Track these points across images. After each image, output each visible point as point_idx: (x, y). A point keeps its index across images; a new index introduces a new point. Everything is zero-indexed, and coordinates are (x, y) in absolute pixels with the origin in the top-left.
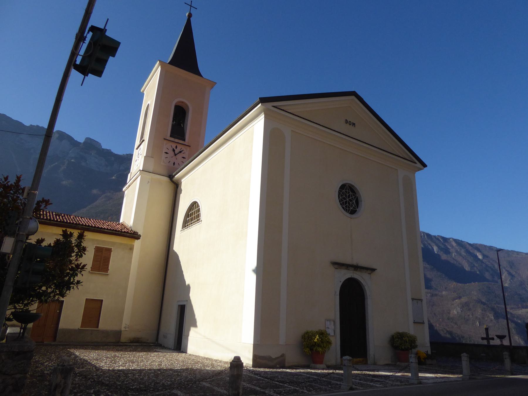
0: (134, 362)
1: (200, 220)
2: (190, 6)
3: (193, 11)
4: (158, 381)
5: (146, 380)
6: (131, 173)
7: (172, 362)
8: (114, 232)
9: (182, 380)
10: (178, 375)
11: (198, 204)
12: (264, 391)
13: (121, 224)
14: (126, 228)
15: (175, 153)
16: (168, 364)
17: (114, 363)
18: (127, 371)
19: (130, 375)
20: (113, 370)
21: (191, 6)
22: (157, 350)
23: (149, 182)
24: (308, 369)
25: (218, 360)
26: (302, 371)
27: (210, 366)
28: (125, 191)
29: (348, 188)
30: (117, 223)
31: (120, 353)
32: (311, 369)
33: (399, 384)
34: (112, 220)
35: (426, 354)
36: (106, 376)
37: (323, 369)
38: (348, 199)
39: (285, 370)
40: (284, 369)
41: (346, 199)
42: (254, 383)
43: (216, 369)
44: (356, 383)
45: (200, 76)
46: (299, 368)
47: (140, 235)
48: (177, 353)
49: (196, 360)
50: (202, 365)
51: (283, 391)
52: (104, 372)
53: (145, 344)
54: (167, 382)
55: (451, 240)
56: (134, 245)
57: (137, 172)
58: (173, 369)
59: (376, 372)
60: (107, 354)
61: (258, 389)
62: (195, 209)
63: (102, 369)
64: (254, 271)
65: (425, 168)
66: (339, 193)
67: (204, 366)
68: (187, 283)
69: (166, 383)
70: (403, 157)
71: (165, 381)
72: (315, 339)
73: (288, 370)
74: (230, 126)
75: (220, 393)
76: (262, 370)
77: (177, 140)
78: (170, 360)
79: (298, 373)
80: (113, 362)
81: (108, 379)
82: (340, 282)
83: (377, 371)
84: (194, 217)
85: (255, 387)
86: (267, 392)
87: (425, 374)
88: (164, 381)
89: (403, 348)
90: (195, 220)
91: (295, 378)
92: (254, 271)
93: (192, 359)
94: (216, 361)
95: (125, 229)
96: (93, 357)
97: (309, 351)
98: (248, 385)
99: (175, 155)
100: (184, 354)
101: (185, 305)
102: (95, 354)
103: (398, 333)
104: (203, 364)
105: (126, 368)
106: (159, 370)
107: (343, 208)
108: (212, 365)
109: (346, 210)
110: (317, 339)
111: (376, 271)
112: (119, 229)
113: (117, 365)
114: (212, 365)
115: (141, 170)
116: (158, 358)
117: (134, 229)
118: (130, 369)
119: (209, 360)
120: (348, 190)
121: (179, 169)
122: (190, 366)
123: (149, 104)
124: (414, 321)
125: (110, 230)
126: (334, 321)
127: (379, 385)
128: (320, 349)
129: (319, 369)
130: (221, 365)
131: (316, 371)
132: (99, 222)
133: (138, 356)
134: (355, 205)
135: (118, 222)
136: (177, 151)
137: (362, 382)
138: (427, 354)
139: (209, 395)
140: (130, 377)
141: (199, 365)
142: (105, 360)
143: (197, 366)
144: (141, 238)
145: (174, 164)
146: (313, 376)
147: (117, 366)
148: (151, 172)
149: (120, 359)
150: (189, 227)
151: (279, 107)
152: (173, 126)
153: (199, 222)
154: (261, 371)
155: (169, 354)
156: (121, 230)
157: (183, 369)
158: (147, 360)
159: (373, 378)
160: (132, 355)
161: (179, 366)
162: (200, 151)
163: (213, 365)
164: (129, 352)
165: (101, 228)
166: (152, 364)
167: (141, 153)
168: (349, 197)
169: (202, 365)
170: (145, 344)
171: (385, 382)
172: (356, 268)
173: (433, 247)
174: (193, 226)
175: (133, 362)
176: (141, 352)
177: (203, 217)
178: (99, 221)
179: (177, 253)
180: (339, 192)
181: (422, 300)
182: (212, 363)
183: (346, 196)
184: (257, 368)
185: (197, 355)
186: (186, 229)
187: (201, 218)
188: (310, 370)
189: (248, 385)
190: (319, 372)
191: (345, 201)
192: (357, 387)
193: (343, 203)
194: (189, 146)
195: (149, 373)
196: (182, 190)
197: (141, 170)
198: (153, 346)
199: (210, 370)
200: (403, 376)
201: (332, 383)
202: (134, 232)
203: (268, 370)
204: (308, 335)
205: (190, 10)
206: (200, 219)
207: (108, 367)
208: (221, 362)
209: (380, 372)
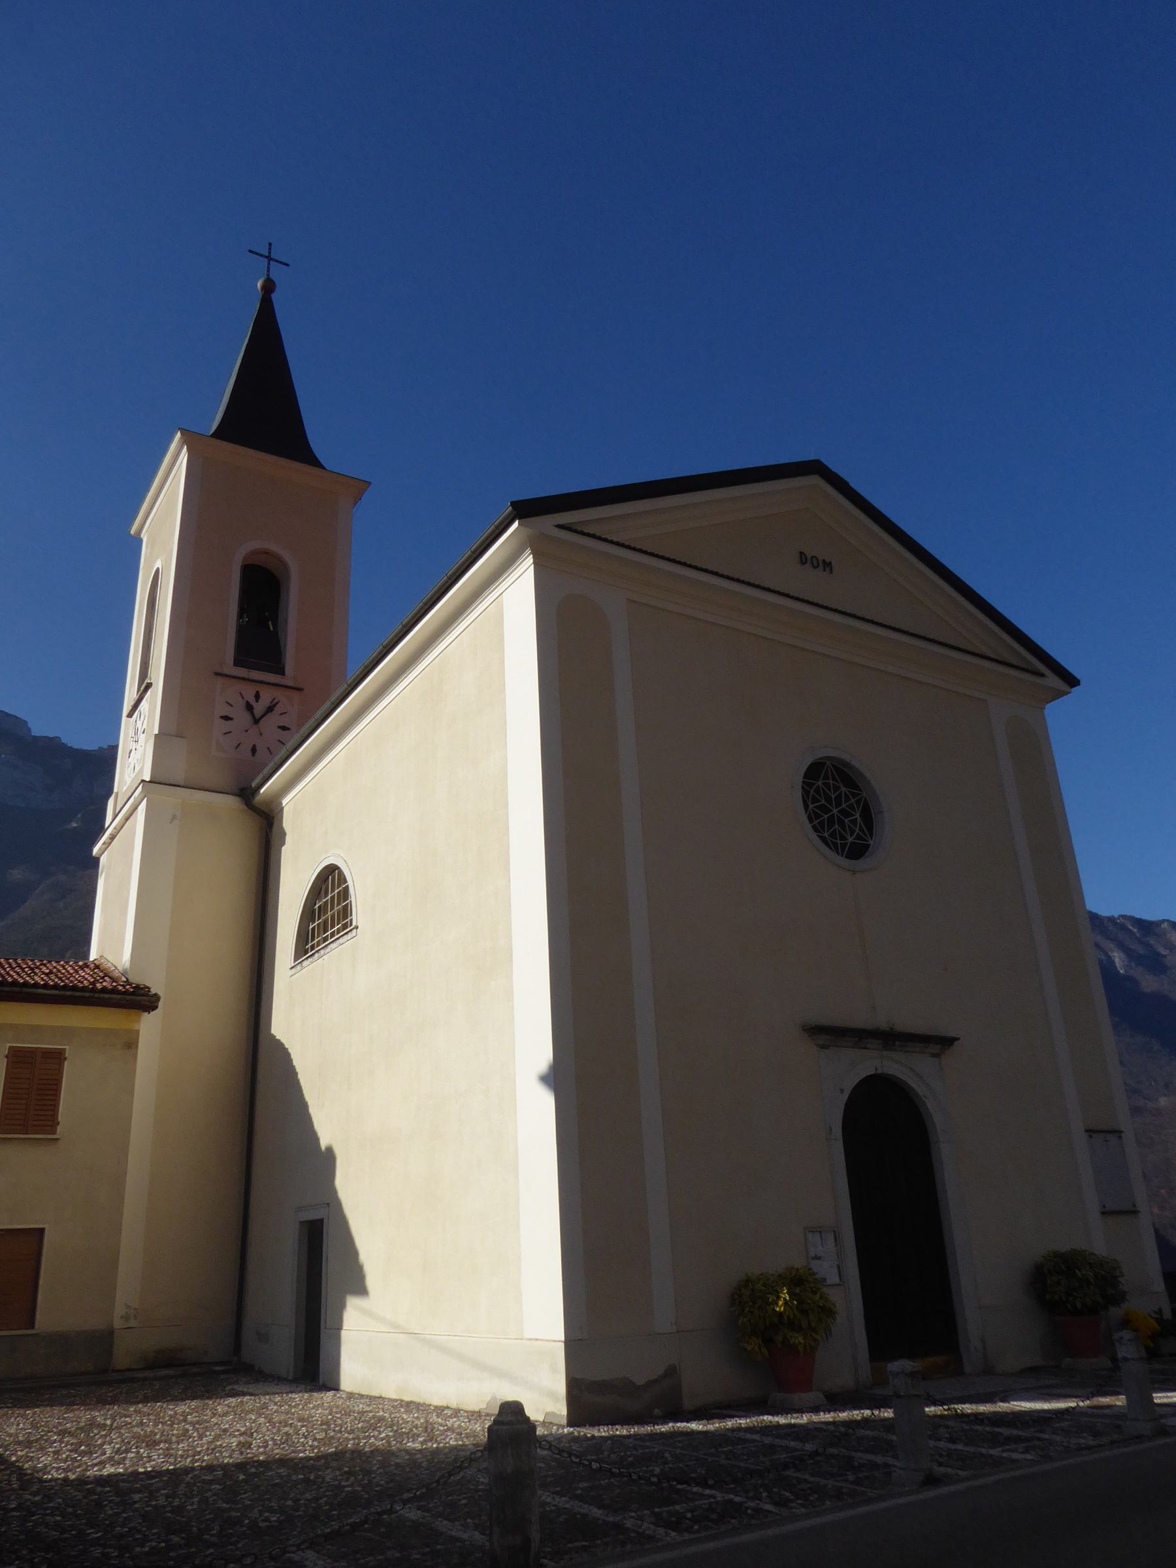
0: (155, 1441)
1: (351, 925)
2: (266, 257)
3: (277, 272)
4: (234, 1514)
5: (192, 1513)
6: (117, 794)
7: (287, 1429)
8: (69, 993)
9: (322, 1501)
10: (307, 1481)
11: (341, 873)
12: (618, 1519)
13: (92, 966)
14: (110, 977)
15: (253, 715)
16: (273, 1439)
17: (83, 1454)
18: (129, 1482)
19: (137, 1497)
20: (82, 1482)
21: (269, 258)
22: (236, 1387)
23: (174, 817)
24: (763, 1414)
25: (448, 1407)
26: (743, 1422)
27: (418, 1436)
28: (101, 855)
29: (832, 774)
30: (81, 963)
31: (108, 1411)
32: (772, 1415)
33: (1091, 1442)
34: (59, 956)
35: (1156, 1319)
36: (52, 1508)
37: (816, 1410)
38: (835, 811)
39: (685, 1424)
40: (682, 1422)
41: (830, 811)
42: (579, 1492)
43: (441, 1445)
44: (941, 1456)
45: (315, 465)
46: (733, 1413)
47: (156, 995)
48: (306, 1392)
49: (371, 1415)
50: (391, 1434)
51: (689, 1515)
52: (49, 1490)
53: (195, 1370)
54: (266, 1514)
55: (1165, 925)
56: (138, 1032)
57: (134, 788)
58: (292, 1460)
59: (1001, 1404)
60: (64, 1418)
61: (596, 1512)
62: (333, 890)
63: (41, 1481)
64: (545, 1079)
65: (1072, 689)
66: (806, 793)
67: (399, 1435)
68: (323, 1144)
69: (263, 1521)
70: (1000, 659)
71: (260, 1512)
72: (777, 1305)
73: (694, 1426)
74: (425, 604)
75: (458, 1544)
76: (603, 1434)
77: (256, 675)
78: (280, 1423)
79: (729, 1434)
80: (83, 1448)
81: (59, 1518)
82: (842, 1091)
83: (1004, 1400)
84: (333, 917)
85: (586, 1506)
86: (629, 1524)
87: (1169, 1394)
88: (256, 1510)
89: (1079, 1305)
90: (336, 927)
91: (723, 1457)
92: (545, 1079)
93: (359, 1413)
94: (440, 1410)
95: (105, 981)
96: (17, 1435)
97: (760, 1348)
98: (562, 1502)
99: (256, 721)
100: (331, 1393)
101: (322, 1221)
102: (24, 1424)
103: (1057, 1255)
104: (395, 1428)
105: (126, 1469)
106: (240, 1467)
107: (823, 839)
108: (428, 1428)
109: (834, 847)
110: (786, 1303)
111: (956, 1043)
112: (85, 982)
113: (97, 1457)
114: (426, 1431)
115: (148, 779)
116: (241, 1418)
117: (136, 979)
118: (141, 1470)
119: (418, 1410)
120: (834, 779)
121: (271, 765)
122: (350, 1440)
123: (158, 570)
124: (1104, 1206)
125: (56, 987)
126: (835, 1232)
127: (1022, 1453)
128: (798, 1339)
129: (801, 1411)
130: (460, 1426)
131: (793, 1421)
132: (19, 966)
133: (171, 1416)
134: (861, 829)
135: (82, 959)
136: (259, 708)
137: (960, 1447)
138: (1160, 1320)
139: (418, 1556)
140: (137, 1506)
141: (383, 1435)
142: (55, 1441)
143: (376, 1438)
144: (161, 1004)
145: (254, 750)
146: (784, 1442)
147: (96, 1465)
148: (179, 786)
149: (106, 1436)
150: (318, 951)
151: (579, 529)
152: (241, 631)
153: (347, 933)
154: (602, 1437)
155: (278, 1398)
156: (91, 983)
157: (325, 1457)
158: (201, 1431)
159: (997, 1430)
160: (149, 1415)
161: (310, 1443)
162: (333, 698)
163: (433, 1429)
164: (140, 1406)
165: (26, 984)
166: (218, 1443)
167: (145, 726)
168: (838, 804)
169: (391, 1434)
170: (195, 1370)
171: (1039, 1439)
172: (890, 1039)
173: (1110, 953)
174: (330, 947)
175: (152, 1444)
176: (183, 1400)
177: (359, 915)
178: (17, 963)
179: (282, 1044)
180: (803, 787)
181: (1122, 1132)
182: (427, 1421)
183: (828, 799)
184: (585, 1426)
185: (375, 1393)
186: (309, 960)
187: (354, 917)
188: (770, 1418)
189: (562, 1502)
190: (801, 1422)
191: (826, 816)
192: (950, 1470)
193: (822, 823)
194: (300, 690)
195: (204, 1481)
196: (284, 834)
197: (148, 779)
198: (223, 1372)
199: (420, 1451)
200: (1092, 1411)
201: (856, 1464)
202: (138, 987)
203: (625, 1432)
204: (753, 1290)
205: (268, 271)
206: (351, 920)
207: (66, 1470)
208: (457, 1412)
209: (1013, 1401)
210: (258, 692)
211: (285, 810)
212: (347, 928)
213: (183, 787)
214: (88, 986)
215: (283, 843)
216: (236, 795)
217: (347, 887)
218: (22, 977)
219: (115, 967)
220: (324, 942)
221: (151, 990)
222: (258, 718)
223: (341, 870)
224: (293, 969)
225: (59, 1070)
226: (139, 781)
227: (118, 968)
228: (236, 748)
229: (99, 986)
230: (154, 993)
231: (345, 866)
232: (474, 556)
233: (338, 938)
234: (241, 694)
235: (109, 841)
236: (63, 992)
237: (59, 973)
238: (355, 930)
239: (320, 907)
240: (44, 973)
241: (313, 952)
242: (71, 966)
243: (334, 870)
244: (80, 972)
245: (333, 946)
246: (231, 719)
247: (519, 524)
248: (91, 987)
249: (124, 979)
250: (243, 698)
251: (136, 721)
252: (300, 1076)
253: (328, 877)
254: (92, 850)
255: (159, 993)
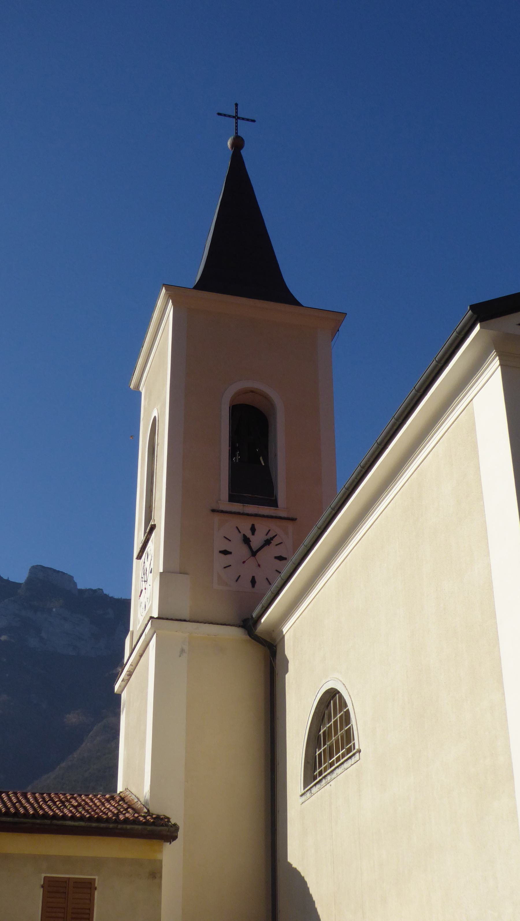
1: (354, 749)
8: (94, 825)
11: (341, 697)
13: (118, 798)
14: (133, 809)
21: (237, 118)
23: (182, 651)
28: (122, 692)
30: (107, 796)
47: (175, 825)
56: (161, 861)
62: (335, 715)
77: (251, 509)
84: (337, 742)
90: (341, 752)
95: (128, 812)
99: (254, 554)
112: (109, 814)
115: (156, 615)
117: (156, 810)
121: (269, 595)
123: (155, 417)
125: (82, 818)
132: (51, 799)
136: (256, 541)
144: (180, 834)
145: (253, 582)
148: (185, 621)
165: (55, 816)
167: (152, 566)
186: (318, 786)
187: (356, 741)
194: (293, 520)
197: (156, 615)
202: (158, 817)
205: (237, 130)
206: (354, 744)
210: (253, 526)
211: (286, 638)
212: (351, 751)
213: (189, 621)
214: (111, 818)
215: (287, 671)
216: (239, 627)
217: (348, 710)
218: (52, 810)
219: (138, 799)
220: (331, 767)
221: (171, 820)
222: (255, 550)
223: (341, 695)
224: (303, 796)
225: (90, 899)
226: (148, 618)
227: (141, 800)
228: (237, 581)
229: (121, 817)
230: (173, 823)
231: (343, 687)
232: (440, 365)
233: (343, 763)
234: (276, 545)
235: (127, 678)
236: (90, 824)
237: (86, 806)
238: (358, 754)
239: (324, 733)
240: (73, 806)
241: (320, 778)
242: (98, 799)
243: (335, 695)
244: (106, 804)
245: (338, 771)
246: (230, 553)
247: (481, 327)
248: (114, 818)
249: (145, 810)
250: (240, 532)
251: (144, 563)
252: (317, 905)
253: (330, 702)
254: (114, 687)
255: (178, 824)
